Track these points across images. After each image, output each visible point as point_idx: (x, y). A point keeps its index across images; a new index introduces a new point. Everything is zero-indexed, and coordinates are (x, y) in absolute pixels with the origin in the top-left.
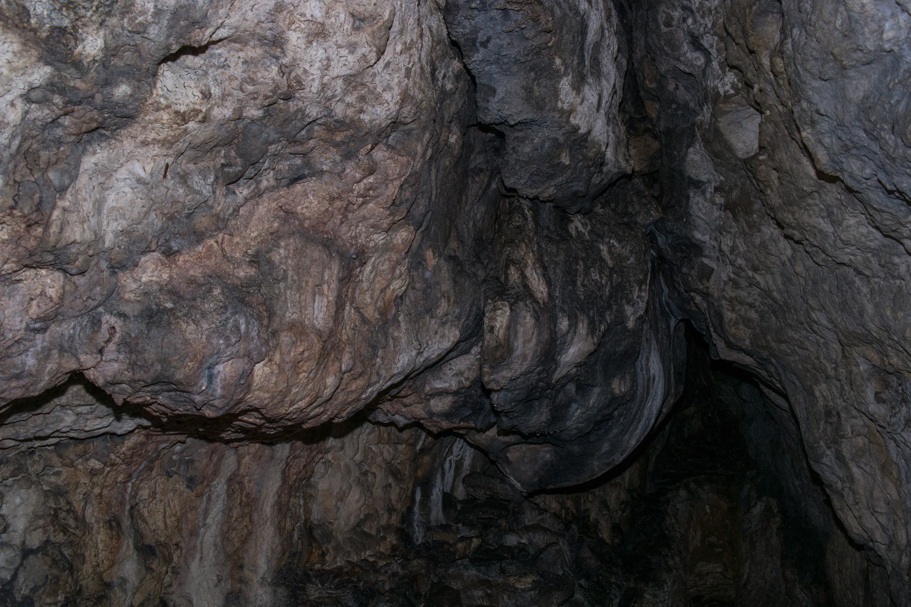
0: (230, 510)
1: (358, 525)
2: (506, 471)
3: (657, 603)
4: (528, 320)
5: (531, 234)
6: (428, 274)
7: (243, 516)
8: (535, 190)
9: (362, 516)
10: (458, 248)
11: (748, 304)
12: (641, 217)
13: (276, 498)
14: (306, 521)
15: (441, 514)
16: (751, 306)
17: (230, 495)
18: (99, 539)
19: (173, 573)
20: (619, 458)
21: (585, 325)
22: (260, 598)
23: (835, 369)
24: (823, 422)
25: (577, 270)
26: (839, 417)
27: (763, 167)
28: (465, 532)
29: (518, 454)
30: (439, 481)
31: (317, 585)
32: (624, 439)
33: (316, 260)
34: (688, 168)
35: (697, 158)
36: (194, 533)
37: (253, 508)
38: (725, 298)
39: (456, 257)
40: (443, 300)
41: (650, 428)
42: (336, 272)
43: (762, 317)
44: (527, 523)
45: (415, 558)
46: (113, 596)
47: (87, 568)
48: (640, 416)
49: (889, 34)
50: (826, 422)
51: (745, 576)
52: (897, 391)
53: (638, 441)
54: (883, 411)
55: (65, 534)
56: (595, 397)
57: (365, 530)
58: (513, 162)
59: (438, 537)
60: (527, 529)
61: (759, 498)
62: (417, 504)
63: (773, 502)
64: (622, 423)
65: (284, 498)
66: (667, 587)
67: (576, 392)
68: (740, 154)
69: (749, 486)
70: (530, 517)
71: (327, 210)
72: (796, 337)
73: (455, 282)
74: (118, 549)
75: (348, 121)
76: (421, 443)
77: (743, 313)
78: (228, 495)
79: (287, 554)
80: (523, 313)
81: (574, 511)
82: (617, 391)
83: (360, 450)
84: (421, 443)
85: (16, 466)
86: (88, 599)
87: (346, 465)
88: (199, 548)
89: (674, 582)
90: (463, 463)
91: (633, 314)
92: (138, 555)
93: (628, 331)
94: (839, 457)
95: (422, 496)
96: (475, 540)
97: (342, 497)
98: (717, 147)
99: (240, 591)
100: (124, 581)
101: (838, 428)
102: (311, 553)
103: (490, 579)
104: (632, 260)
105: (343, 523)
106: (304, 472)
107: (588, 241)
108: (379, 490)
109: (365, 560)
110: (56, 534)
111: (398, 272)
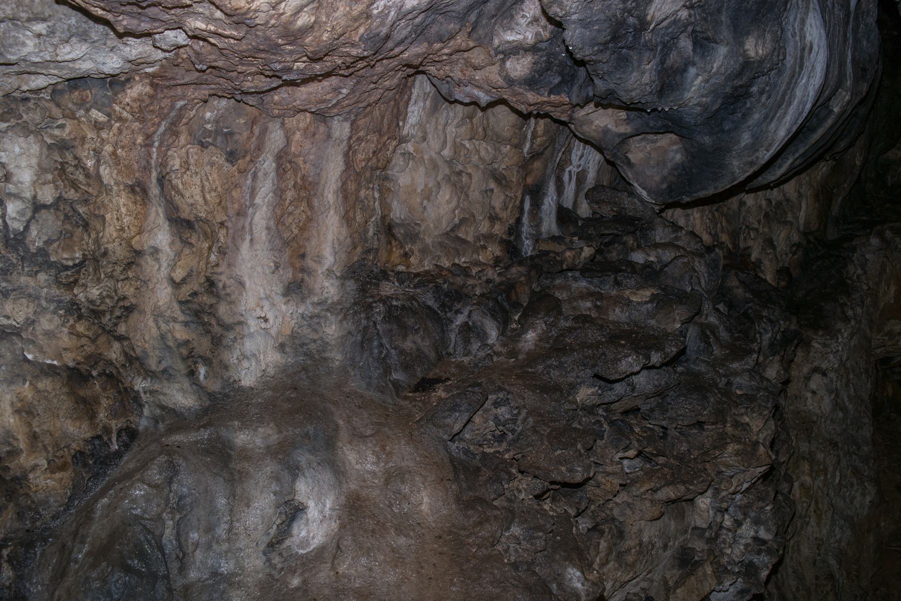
0: (283, 191)
1: (452, 230)
2: (628, 176)
3: (826, 353)
7: (299, 199)
9: (457, 220)
13: (340, 184)
14: (383, 218)
15: (554, 226)
17: (281, 171)
18: (121, 203)
19: (219, 252)
20: (765, 156)
22: (326, 290)
31: (393, 283)
32: (770, 128)
36: (241, 213)
37: (312, 193)
41: (805, 115)
44: (658, 240)
46: (143, 263)
47: (111, 231)
48: (790, 98)
53: (789, 131)
55: (76, 191)
57: (460, 235)
60: (656, 246)
64: (764, 105)
65: (351, 186)
67: (694, 50)
70: (660, 234)
74: (146, 216)
76: (528, 145)
78: (278, 174)
79: (359, 249)
81: (730, 246)
82: (752, 53)
83: (449, 145)
84: (528, 145)
85: (6, 110)
86: (116, 263)
87: (431, 160)
88: (247, 229)
89: (852, 335)
90: (586, 176)
92: (170, 226)
95: (531, 205)
97: (428, 195)
99: (302, 280)
100: (156, 251)
102: (390, 252)
103: (603, 292)
105: (432, 225)
106: (374, 160)
108: (477, 193)
110: (66, 190)
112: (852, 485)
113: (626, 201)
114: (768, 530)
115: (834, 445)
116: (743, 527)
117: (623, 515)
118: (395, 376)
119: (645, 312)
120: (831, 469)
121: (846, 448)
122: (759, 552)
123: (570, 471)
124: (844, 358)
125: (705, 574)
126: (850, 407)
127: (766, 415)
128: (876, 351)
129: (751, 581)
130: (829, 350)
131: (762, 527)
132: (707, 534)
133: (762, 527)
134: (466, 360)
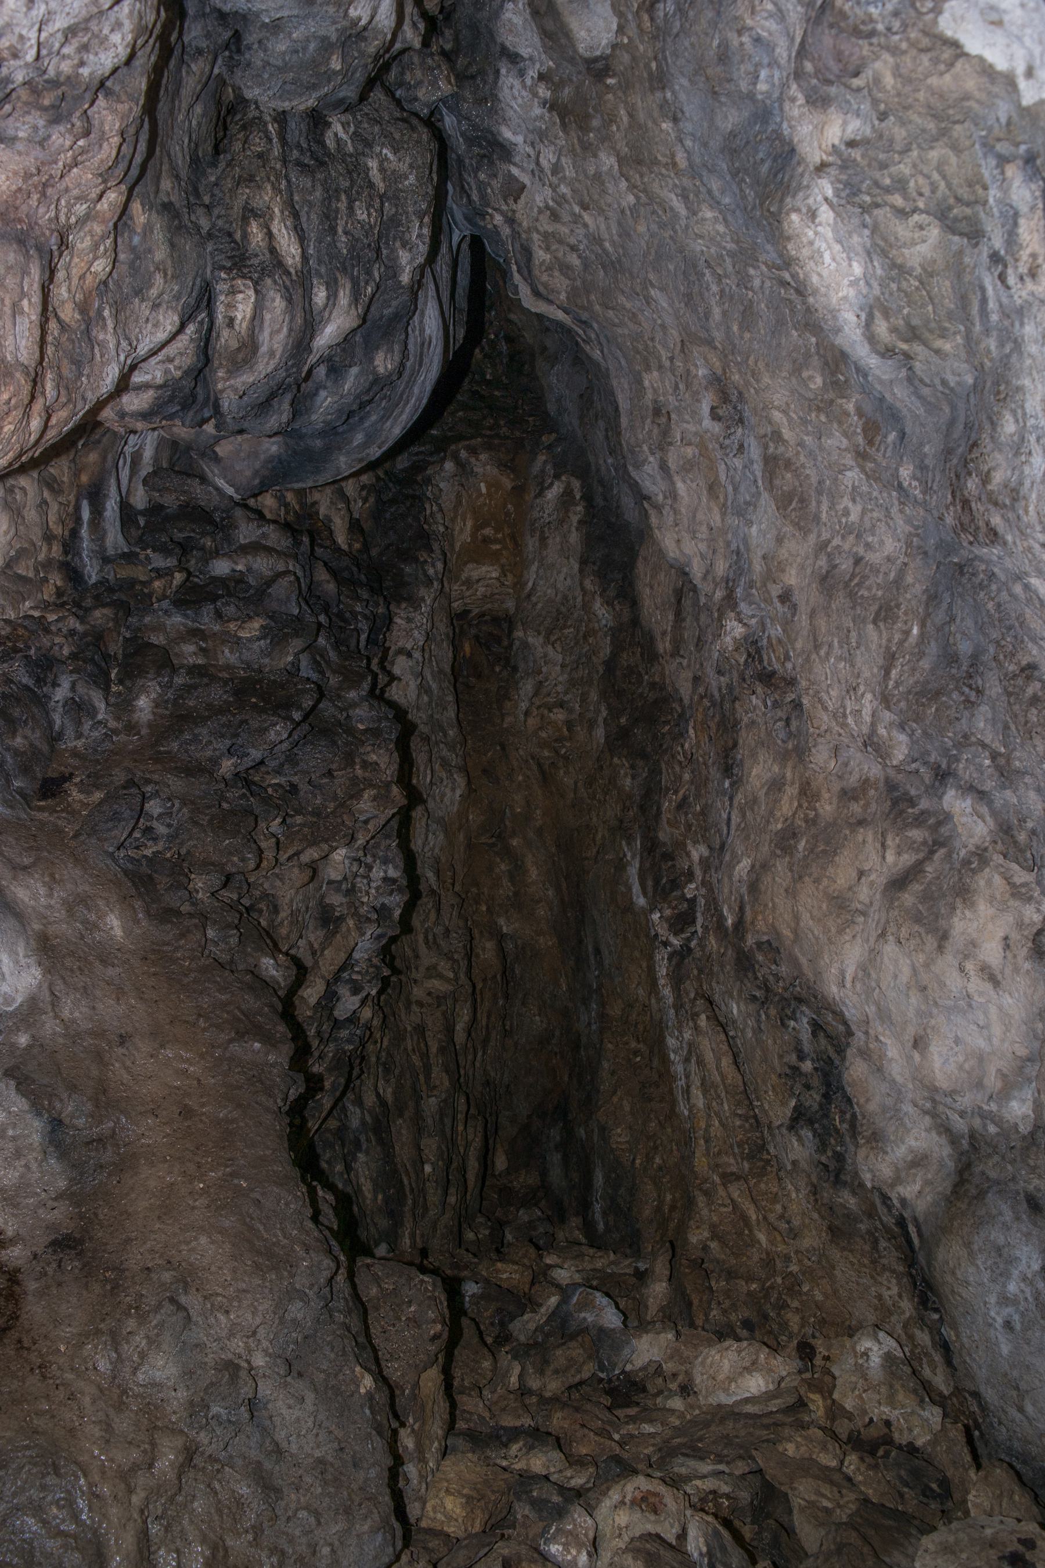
4: (277, 303)
5: (278, 166)
6: (136, 240)
8: (287, 104)
10: (173, 188)
11: (568, 245)
12: (424, 90)
15: (120, 537)
16: (573, 248)
21: (347, 292)
23: (672, 359)
24: (649, 421)
25: (337, 210)
26: (669, 419)
27: (610, 96)
28: (159, 561)
29: (230, 447)
30: (113, 490)
33: (11, 267)
34: (502, 30)
35: (518, 20)
38: (538, 232)
39: (171, 203)
40: (158, 276)
42: (37, 279)
43: (586, 266)
45: (96, 607)
49: (762, 87)
50: (653, 422)
51: (530, 584)
52: (735, 408)
54: (717, 429)
56: (352, 380)
58: (259, 63)
59: (125, 572)
61: (557, 476)
62: (85, 525)
63: (576, 484)
67: (327, 375)
68: (581, 48)
69: (544, 458)
70: (246, 532)
71: (20, 189)
72: (628, 305)
73: (172, 245)
75: (62, 79)
77: (560, 255)
80: (272, 293)
81: (297, 507)
82: (381, 370)
91: (410, 263)
93: (403, 287)
94: (664, 467)
96: (177, 575)
98: (550, 25)
101: (666, 432)
104: (412, 179)
107: (351, 155)
108: (33, 512)
109: (27, 617)
111: (102, 248)
113: (197, 489)
114: (396, 867)
117: (273, 887)
118: (17, 784)
119: (258, 651)
123: (243, 860)
125: (349, 930)
126: (434, 686)
132: (344, 886)
134: (79, 744)
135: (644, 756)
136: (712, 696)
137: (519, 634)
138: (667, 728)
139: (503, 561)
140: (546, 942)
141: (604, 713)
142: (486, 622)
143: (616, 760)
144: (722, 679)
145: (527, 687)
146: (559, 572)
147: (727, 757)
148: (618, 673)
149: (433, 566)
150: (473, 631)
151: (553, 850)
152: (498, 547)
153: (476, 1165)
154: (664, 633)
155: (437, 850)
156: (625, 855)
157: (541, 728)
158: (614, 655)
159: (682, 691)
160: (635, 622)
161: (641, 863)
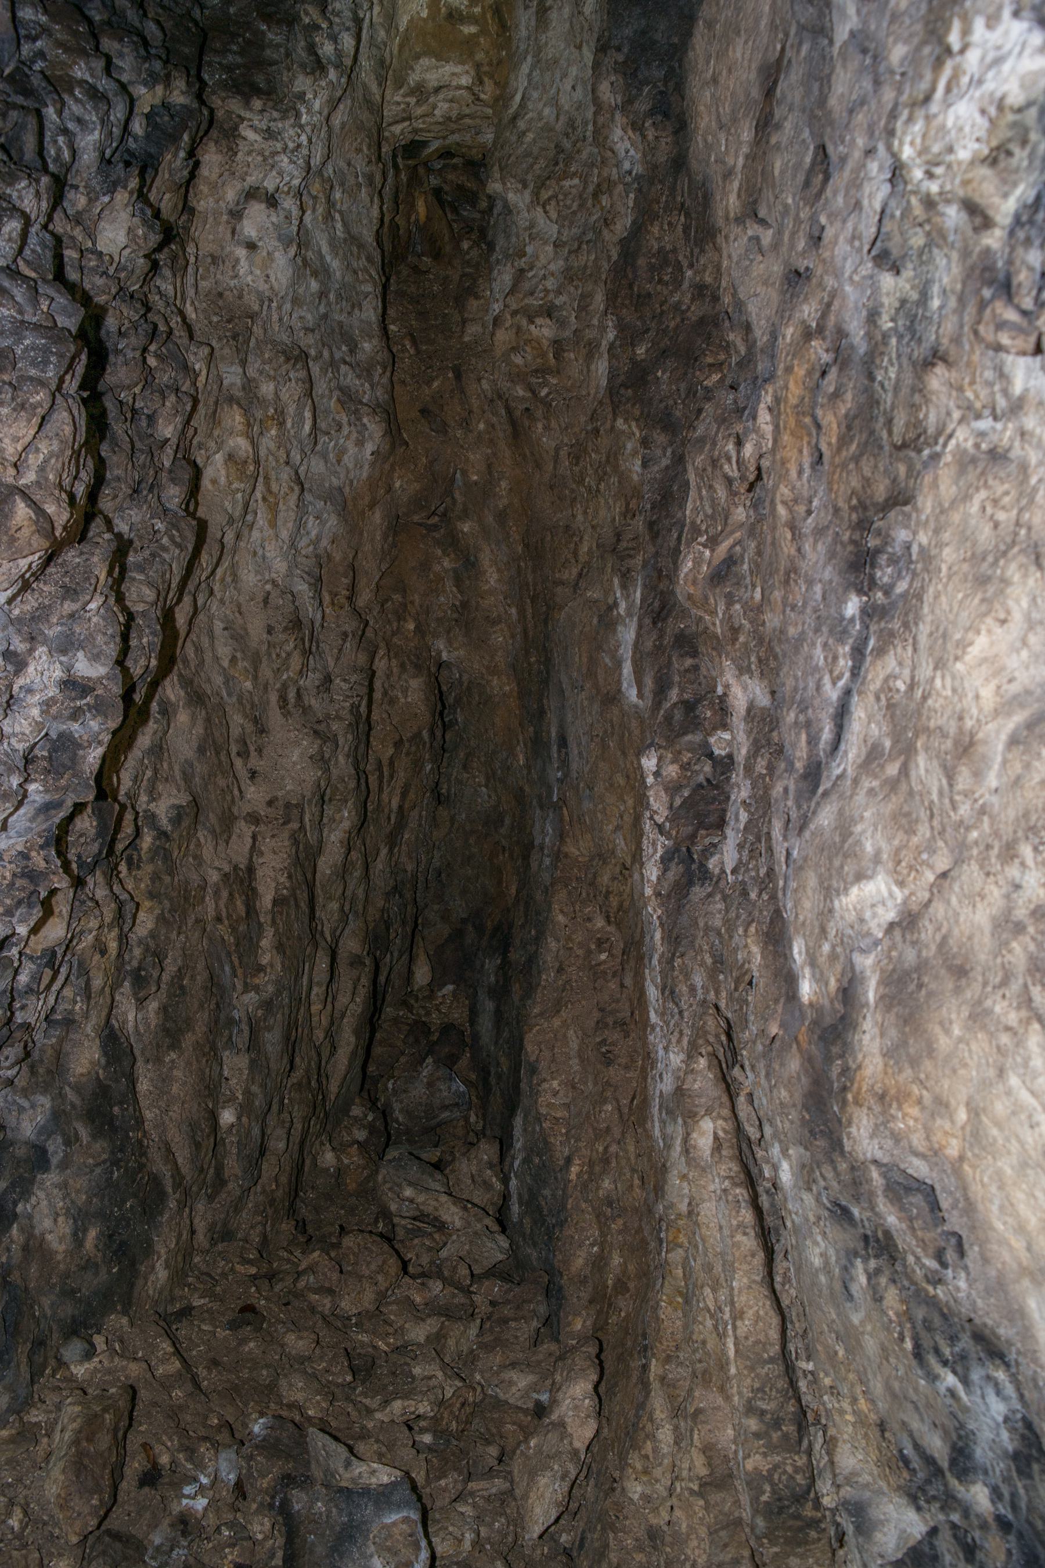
3: (275, 154)
51: (518, 98)
66: (309, 111)
89: (333, 104)
112: (340, 427)
114: (95, 658)
115: (299, 357)
116: (31, 669)
120: (291, 409)
121: (326, 354)
122: (75, 715)
124: (316, 161)
126: (335, 264)
127: (40, 404)
128: (393, 128)
129: (63, 782)
130: (279, 146)
131: (80, 654)
133: (80, 654)
135: (668, 424)
136: (841, 333)
137: (495, 186)
138: (716, 377)
139: (480, 56)
140: (501, 686)
141: (611, 335)
142: (455, 167)
143: (620, 423)
144: (887, 280)
145: (504, 277)
146: (565, 75)
147: (863, 525)
148: (641, 262)
149: (334, 39)
150: (434, 181)
151: (520, 549)
152: (473, 29)
153: (353, 1039)
154: (728, 175)
155: (324, 543)
156: (616, 605)
157: (514, 349)
158: (638, 230)
159: (752, 308)
160: (679, 163)
161: (639, 635)
